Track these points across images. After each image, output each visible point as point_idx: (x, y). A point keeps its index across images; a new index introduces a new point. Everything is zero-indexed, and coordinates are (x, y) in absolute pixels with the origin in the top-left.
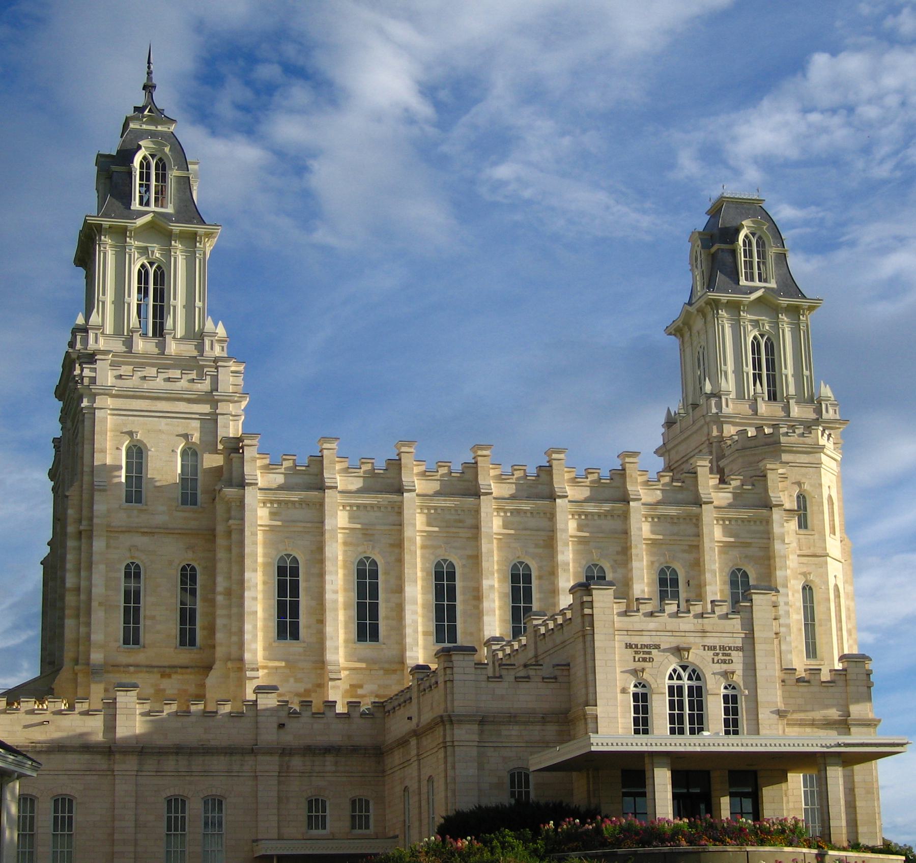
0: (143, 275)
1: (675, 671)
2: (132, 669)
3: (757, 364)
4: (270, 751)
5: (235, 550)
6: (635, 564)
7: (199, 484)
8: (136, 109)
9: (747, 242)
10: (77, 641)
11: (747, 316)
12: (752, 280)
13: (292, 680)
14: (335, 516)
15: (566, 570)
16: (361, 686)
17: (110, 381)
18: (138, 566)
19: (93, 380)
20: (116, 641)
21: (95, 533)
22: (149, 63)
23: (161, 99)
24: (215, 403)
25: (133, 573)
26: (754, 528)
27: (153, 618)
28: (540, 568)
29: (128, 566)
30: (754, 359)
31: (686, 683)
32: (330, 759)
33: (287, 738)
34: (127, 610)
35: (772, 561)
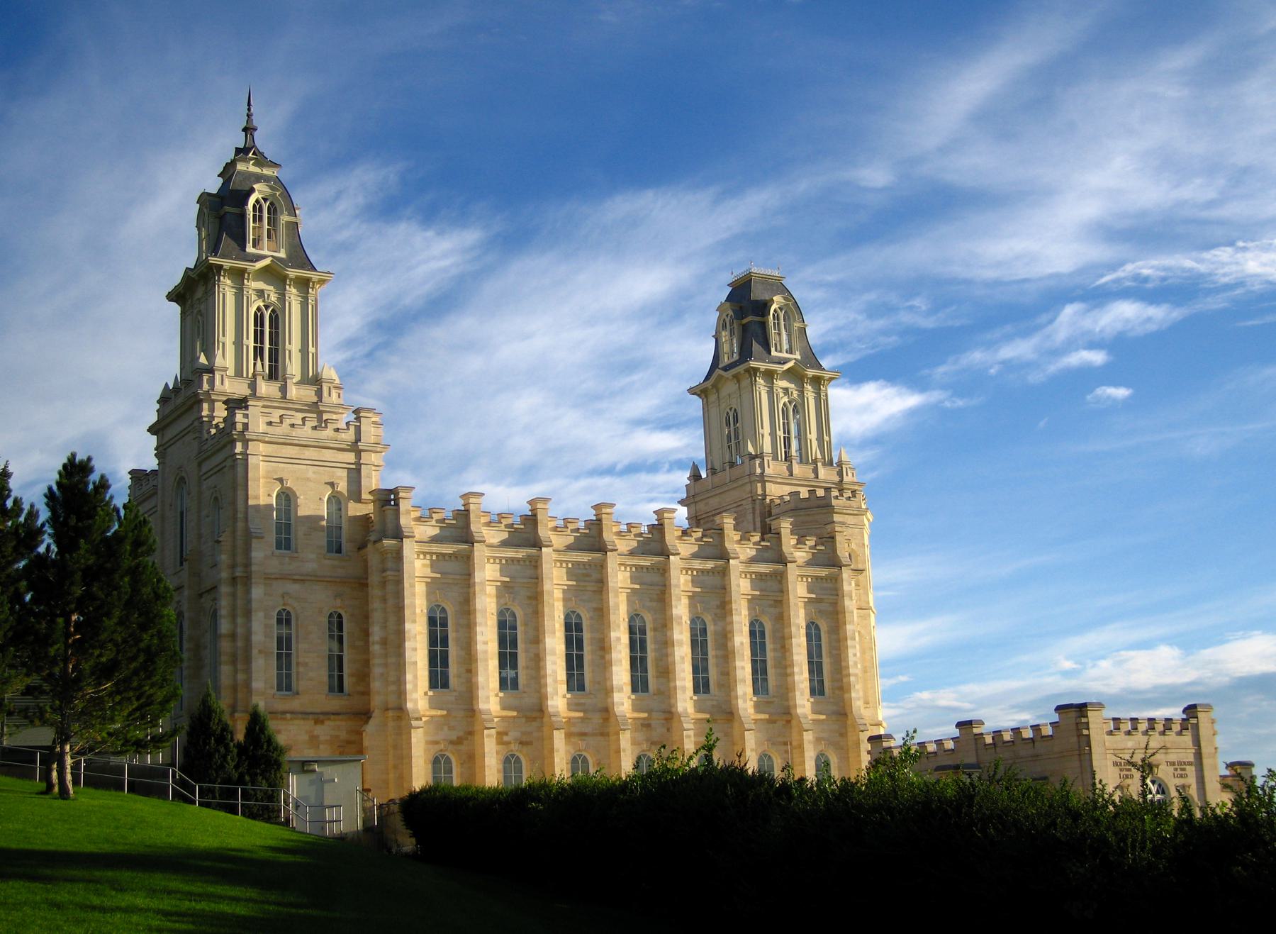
0: (259, 320)
2: (288, 716)
3: (259, 336)
5: (391, 602)
6: (735, 618)
7: (344, 532)
8: (238, 151)
9: (258, 207)
10: (234, 688)
11: (253, 285)
13: (446, 728)
14: (483, 569)
15: (680, 624)
16: (506, 734)
17: (262, 427)
18: (288, 613)
19: (246, 426)
20: (272, 688)
22: (249, 104)
23: (260, 140)
24: (358, 453)
25: (284, 619)
27: (306, 664)
28: (655, 620)
29: (279, 613)
30: (256, 331)
34: (279, 656)
35: (840, 616)
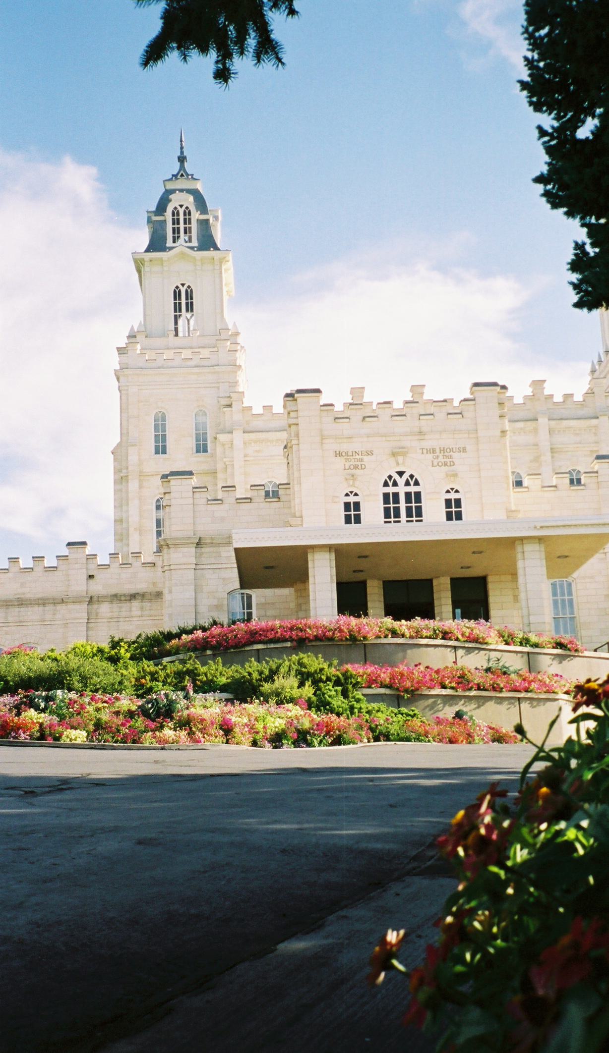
1: (390, 477)
4: (77, 601)
21: (130, 477)
22: (181, 141)
31: (402, 490)
32: (136, 604)
33: (97, 588)
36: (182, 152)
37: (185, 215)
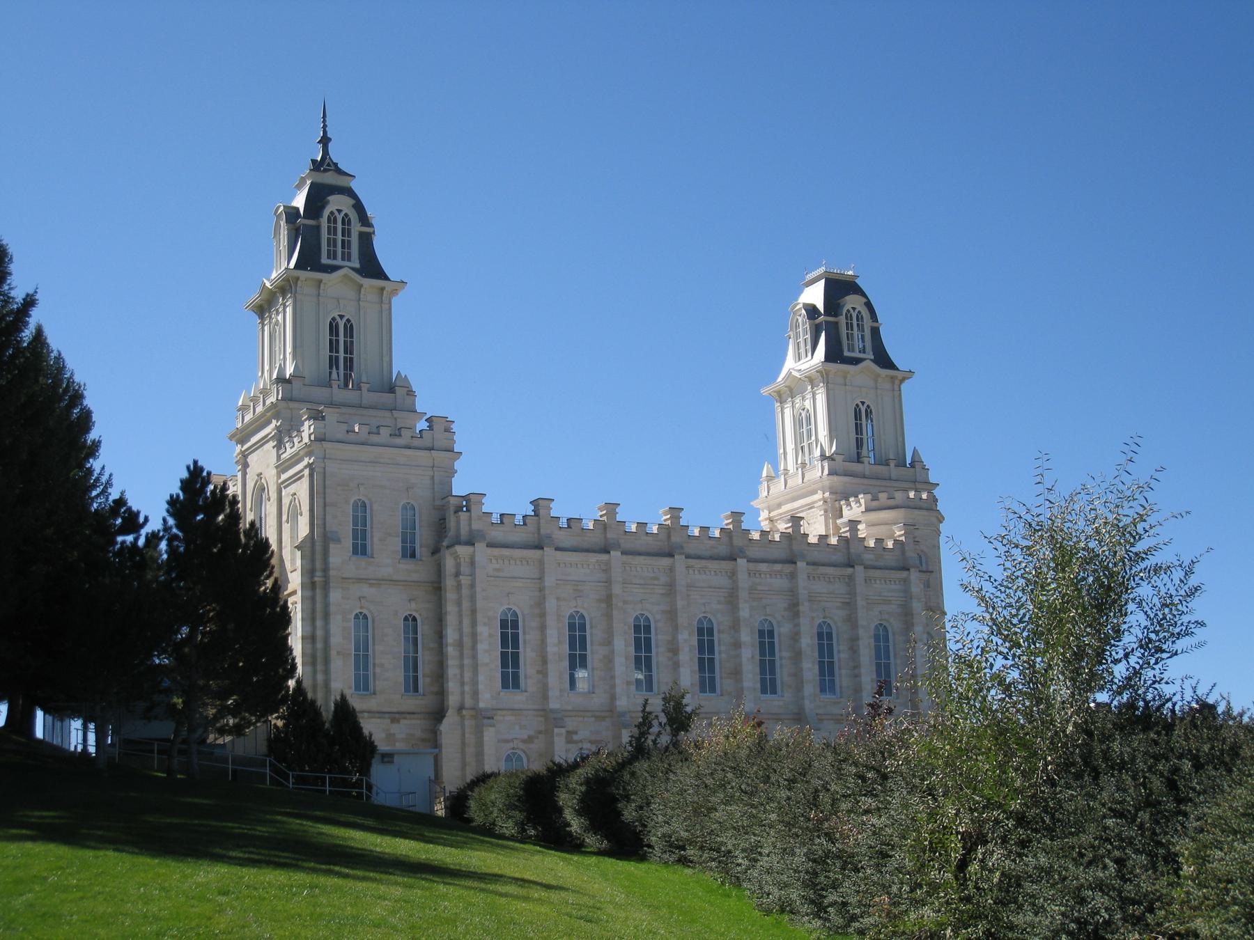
12: (335, 258)
26: (893, 587)
36: (325, 132)
37: (343, 223)
